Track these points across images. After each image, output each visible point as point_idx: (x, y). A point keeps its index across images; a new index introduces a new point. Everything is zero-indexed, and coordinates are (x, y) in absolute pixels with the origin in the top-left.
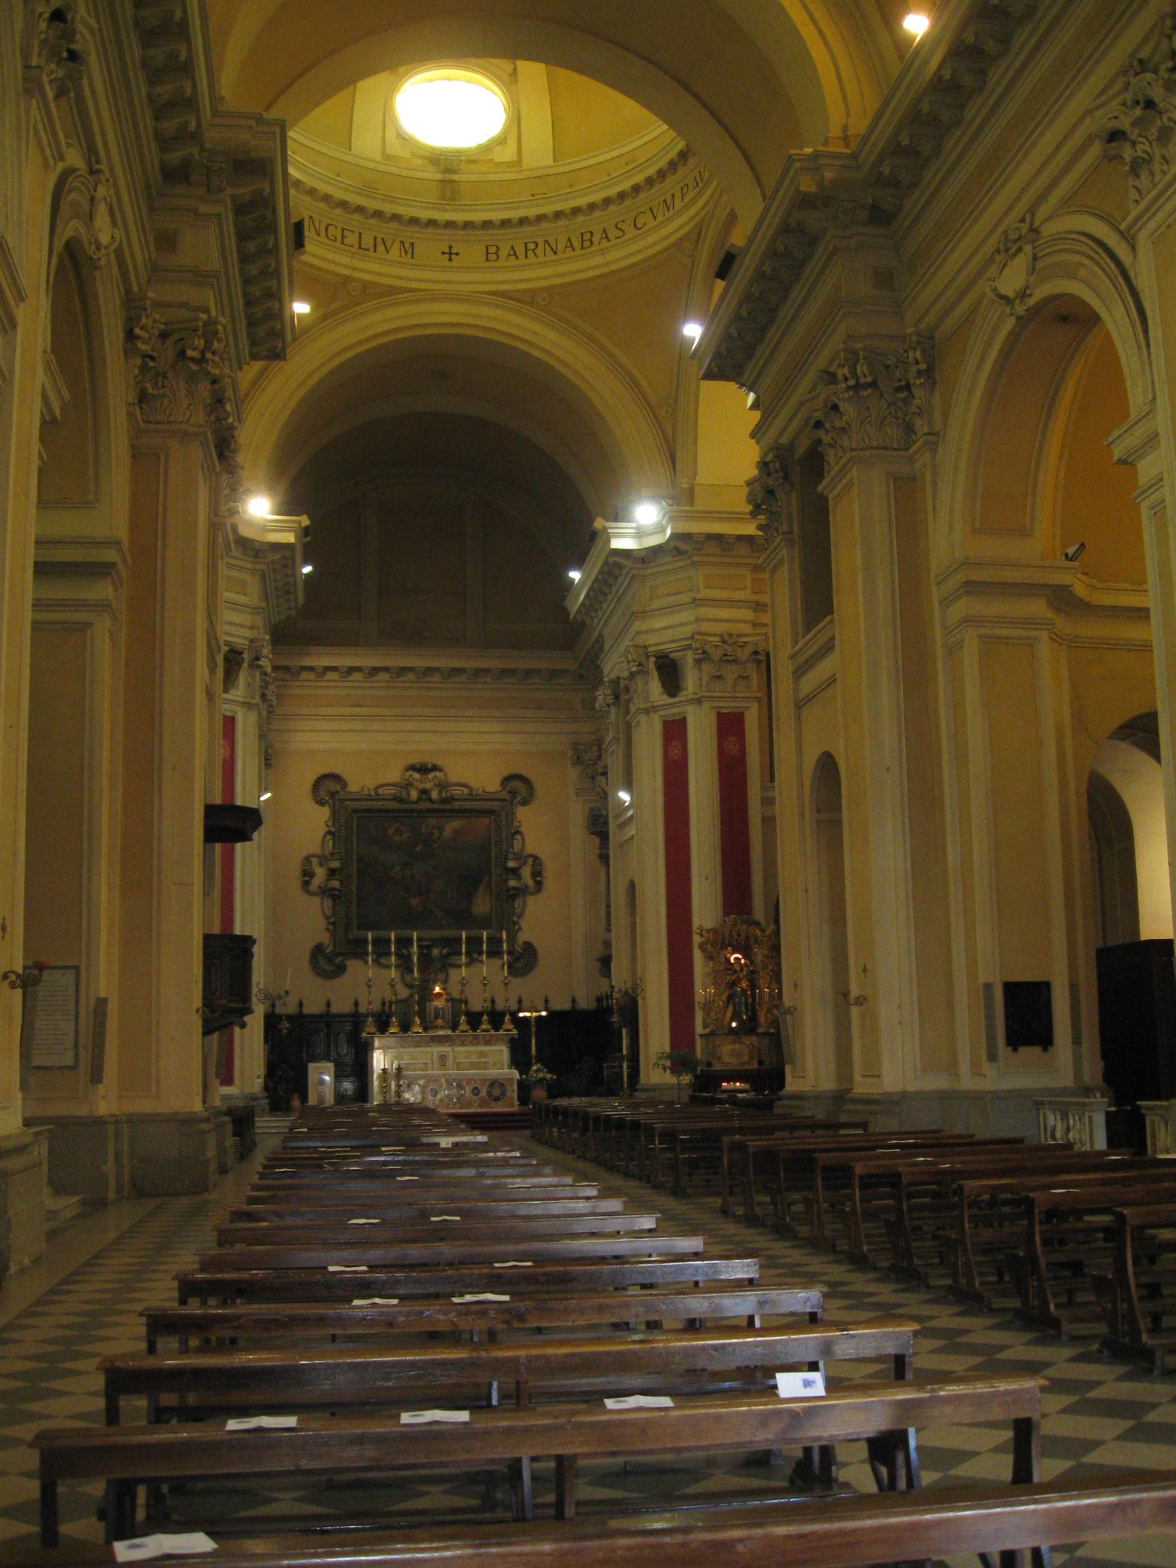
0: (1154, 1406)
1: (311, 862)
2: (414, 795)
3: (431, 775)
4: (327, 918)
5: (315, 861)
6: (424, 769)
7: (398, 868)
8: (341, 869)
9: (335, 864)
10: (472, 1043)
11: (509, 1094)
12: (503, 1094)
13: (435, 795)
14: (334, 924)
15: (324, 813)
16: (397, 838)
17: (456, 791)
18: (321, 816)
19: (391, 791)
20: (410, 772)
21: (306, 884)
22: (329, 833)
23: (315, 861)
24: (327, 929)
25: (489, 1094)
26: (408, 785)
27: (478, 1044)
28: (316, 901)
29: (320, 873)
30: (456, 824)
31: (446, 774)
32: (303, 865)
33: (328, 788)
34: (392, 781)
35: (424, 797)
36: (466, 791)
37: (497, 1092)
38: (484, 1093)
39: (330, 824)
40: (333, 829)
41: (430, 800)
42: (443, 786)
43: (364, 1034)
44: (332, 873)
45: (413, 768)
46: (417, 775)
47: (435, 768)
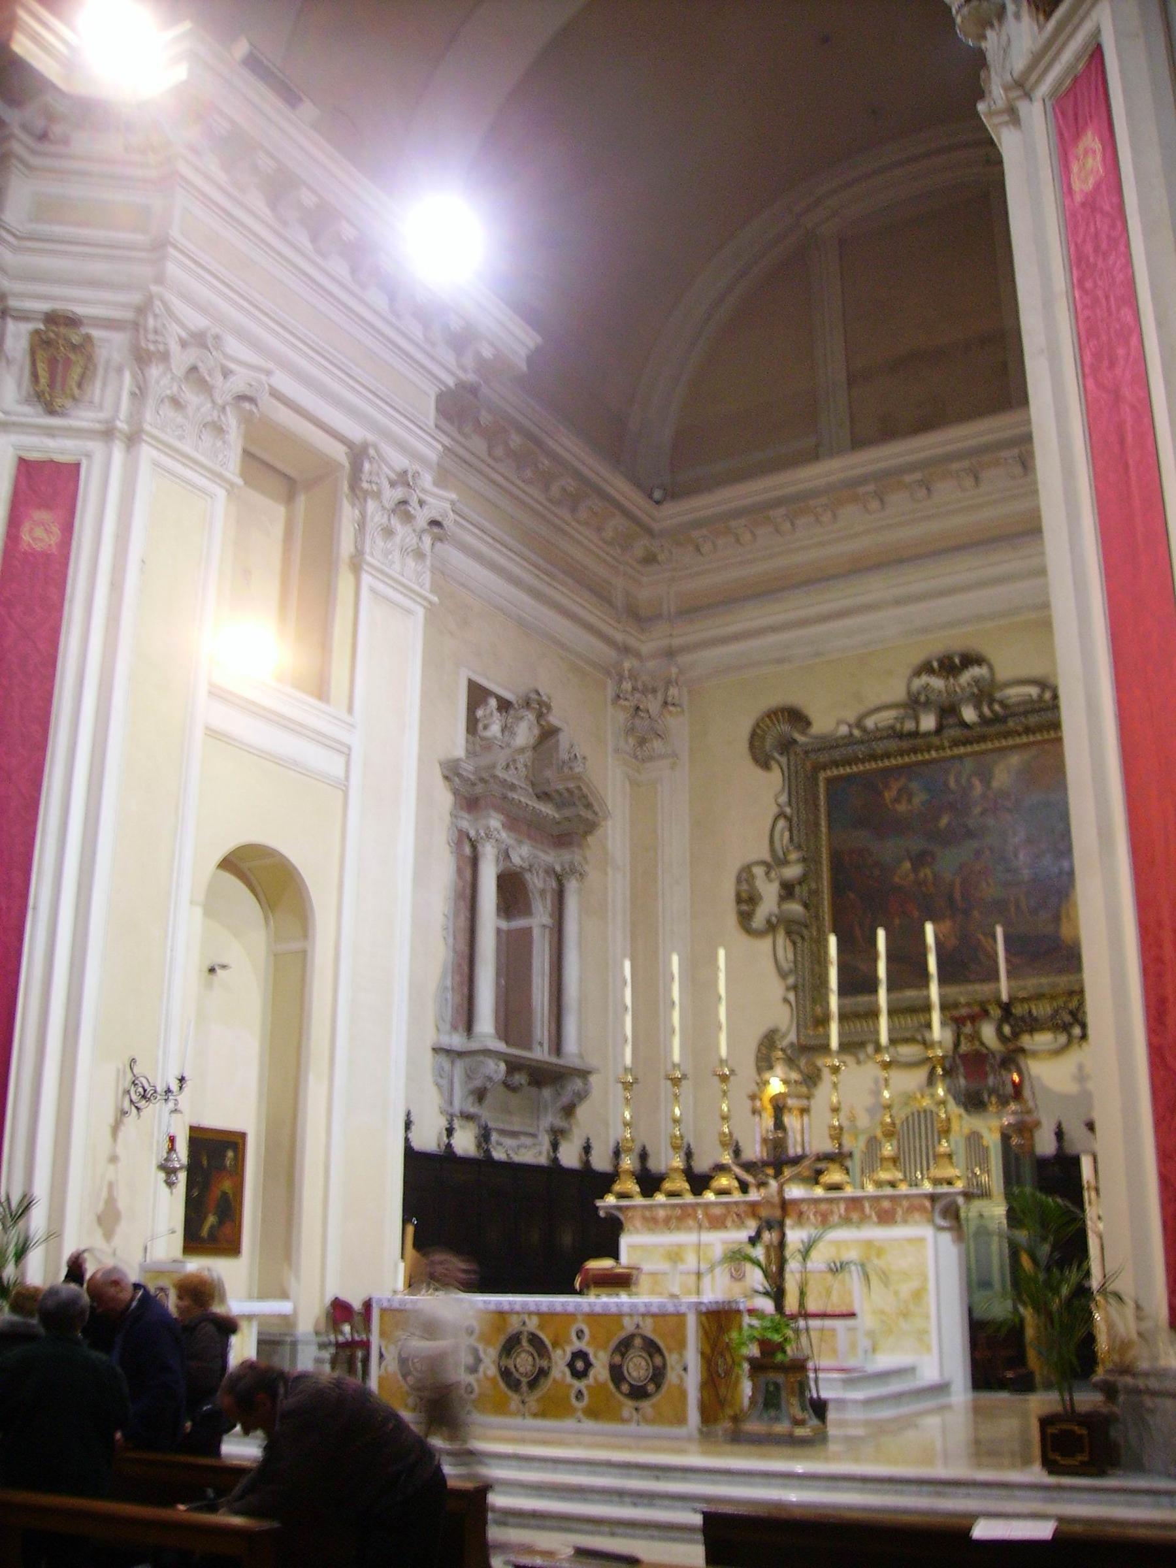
0: (388, 477)
1: (753, 877)
2: (928, 722)
3: (966, 677)
4: (783, 975)
5: (759, 871)
6: (949, 666)
7: (907, 865)
8: (802, 880)
9: (793, 872)
10: (847, 1221)
11: (672, 1376)
12: (658, 1376)
13: (969, 714)
14: (795, 988)
15: (774, 780)
16: (902, 808)
17: (1014, 693)
18: (767, 790)
19: (886, 718)
20: (925, 679)
21: (745, 918)
22: (781, 815)
23: (759, 871)
24: (786, 1000)
25: (617, 1373)
26: (914, 704)
27: (864, 1219)
28: (765, 944)
29: (769, 892)
30: (1015, 760)
31: (991, 667)
32: (739, 881)
33: (780, 735)
34: (887, 698)
35: (951, 720)
36: (1034, 691)
37: (637, 1368)
38: (600, 1371)
39: (783, 799)
40: (788, 810)
41: (964, 725)
42: (984, 694)
43: (611, 1200)
44: (788, 890)
45: (926, 668)
46: (937, 683)
47: (970, 660)
